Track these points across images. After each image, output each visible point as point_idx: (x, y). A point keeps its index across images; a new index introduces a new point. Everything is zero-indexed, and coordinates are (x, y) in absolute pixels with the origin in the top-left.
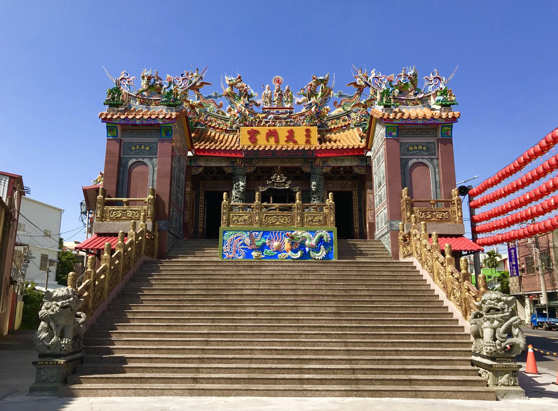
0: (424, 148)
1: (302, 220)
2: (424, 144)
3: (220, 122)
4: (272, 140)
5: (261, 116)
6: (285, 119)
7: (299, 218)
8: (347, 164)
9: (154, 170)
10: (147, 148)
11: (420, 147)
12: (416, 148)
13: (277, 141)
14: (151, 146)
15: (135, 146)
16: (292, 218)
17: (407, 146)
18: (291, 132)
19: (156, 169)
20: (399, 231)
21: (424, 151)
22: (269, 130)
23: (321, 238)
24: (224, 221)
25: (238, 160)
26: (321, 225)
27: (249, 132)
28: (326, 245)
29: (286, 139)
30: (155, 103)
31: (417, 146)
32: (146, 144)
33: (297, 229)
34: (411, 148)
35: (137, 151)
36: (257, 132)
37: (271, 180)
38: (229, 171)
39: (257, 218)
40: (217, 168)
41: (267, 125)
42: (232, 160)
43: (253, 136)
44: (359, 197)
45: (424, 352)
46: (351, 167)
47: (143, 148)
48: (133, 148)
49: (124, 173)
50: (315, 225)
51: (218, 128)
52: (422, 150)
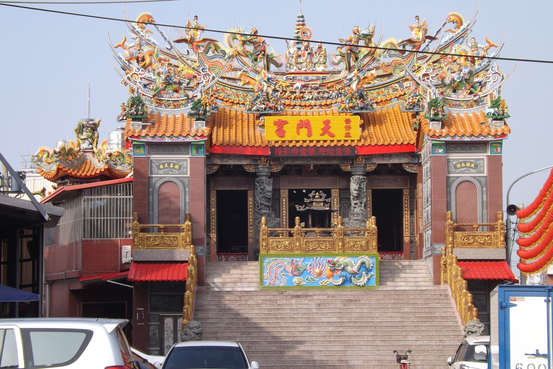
0: (473, 165)
1: (343, 246)
2: (472, 161)
3: (229, 92)
4: (304, 131)
5: (284, 85)
6: (317, 89)
7: (340, 244)
8: (396, 161)
9: (185, 191)
10: (177, 167)
11: (468, 164)
12: (463, 165)
13: (310, 134)
14: (181, 164)
15: (164, 164)
16: (333, 244)
17: (454, 163)
18: (327, 123)
19: (187, 190)
20: (442, 255)
21: (472, 168)
22: (301, 121)
23: (363, 263)
24: (264, 248)
25: (263, 158)
26: (363, 250)
27: (275, 123)
28: (368, 271)
29: (321, 132)
30: (174, 105)
31: (465, 163)
32: (175, 162)
33: (337, 255)
34: (459, 166)
35: (166, 170)
36: (286, 123)
37: (309, 198)
38: (251, 170)
39: (298, 244)
40: (235, 166)
41: (342, 266)
42: (255, 158)
43: (280, 126)
44: (410, 198)
45: (120, 212)
46: (401, 164)
47: (172, 166)
48: (161, 167)
49: (153, 194)
50: (358, 250)
51: (227, 101)
52: (470, 167)
